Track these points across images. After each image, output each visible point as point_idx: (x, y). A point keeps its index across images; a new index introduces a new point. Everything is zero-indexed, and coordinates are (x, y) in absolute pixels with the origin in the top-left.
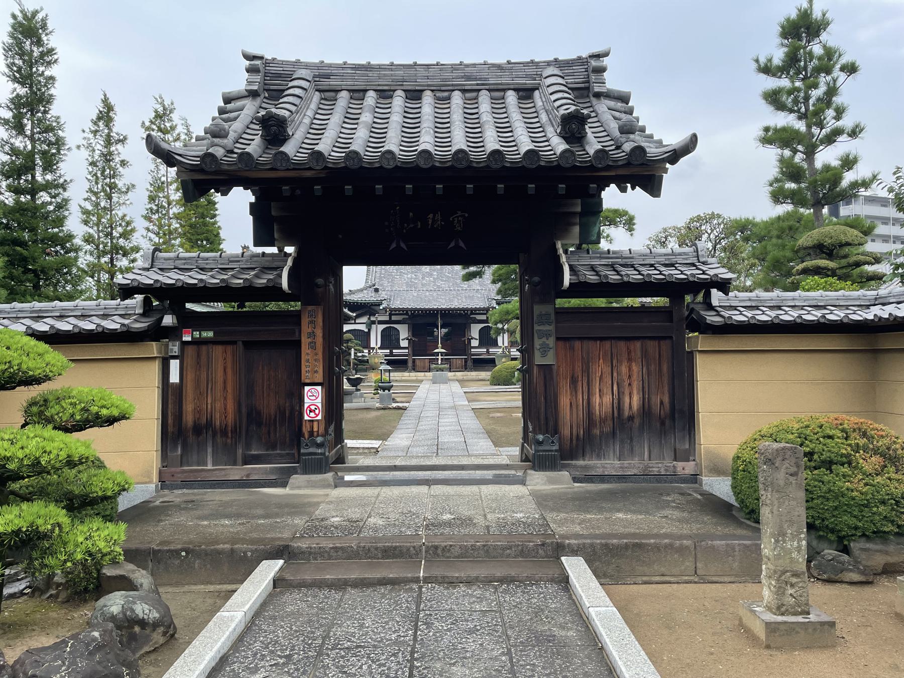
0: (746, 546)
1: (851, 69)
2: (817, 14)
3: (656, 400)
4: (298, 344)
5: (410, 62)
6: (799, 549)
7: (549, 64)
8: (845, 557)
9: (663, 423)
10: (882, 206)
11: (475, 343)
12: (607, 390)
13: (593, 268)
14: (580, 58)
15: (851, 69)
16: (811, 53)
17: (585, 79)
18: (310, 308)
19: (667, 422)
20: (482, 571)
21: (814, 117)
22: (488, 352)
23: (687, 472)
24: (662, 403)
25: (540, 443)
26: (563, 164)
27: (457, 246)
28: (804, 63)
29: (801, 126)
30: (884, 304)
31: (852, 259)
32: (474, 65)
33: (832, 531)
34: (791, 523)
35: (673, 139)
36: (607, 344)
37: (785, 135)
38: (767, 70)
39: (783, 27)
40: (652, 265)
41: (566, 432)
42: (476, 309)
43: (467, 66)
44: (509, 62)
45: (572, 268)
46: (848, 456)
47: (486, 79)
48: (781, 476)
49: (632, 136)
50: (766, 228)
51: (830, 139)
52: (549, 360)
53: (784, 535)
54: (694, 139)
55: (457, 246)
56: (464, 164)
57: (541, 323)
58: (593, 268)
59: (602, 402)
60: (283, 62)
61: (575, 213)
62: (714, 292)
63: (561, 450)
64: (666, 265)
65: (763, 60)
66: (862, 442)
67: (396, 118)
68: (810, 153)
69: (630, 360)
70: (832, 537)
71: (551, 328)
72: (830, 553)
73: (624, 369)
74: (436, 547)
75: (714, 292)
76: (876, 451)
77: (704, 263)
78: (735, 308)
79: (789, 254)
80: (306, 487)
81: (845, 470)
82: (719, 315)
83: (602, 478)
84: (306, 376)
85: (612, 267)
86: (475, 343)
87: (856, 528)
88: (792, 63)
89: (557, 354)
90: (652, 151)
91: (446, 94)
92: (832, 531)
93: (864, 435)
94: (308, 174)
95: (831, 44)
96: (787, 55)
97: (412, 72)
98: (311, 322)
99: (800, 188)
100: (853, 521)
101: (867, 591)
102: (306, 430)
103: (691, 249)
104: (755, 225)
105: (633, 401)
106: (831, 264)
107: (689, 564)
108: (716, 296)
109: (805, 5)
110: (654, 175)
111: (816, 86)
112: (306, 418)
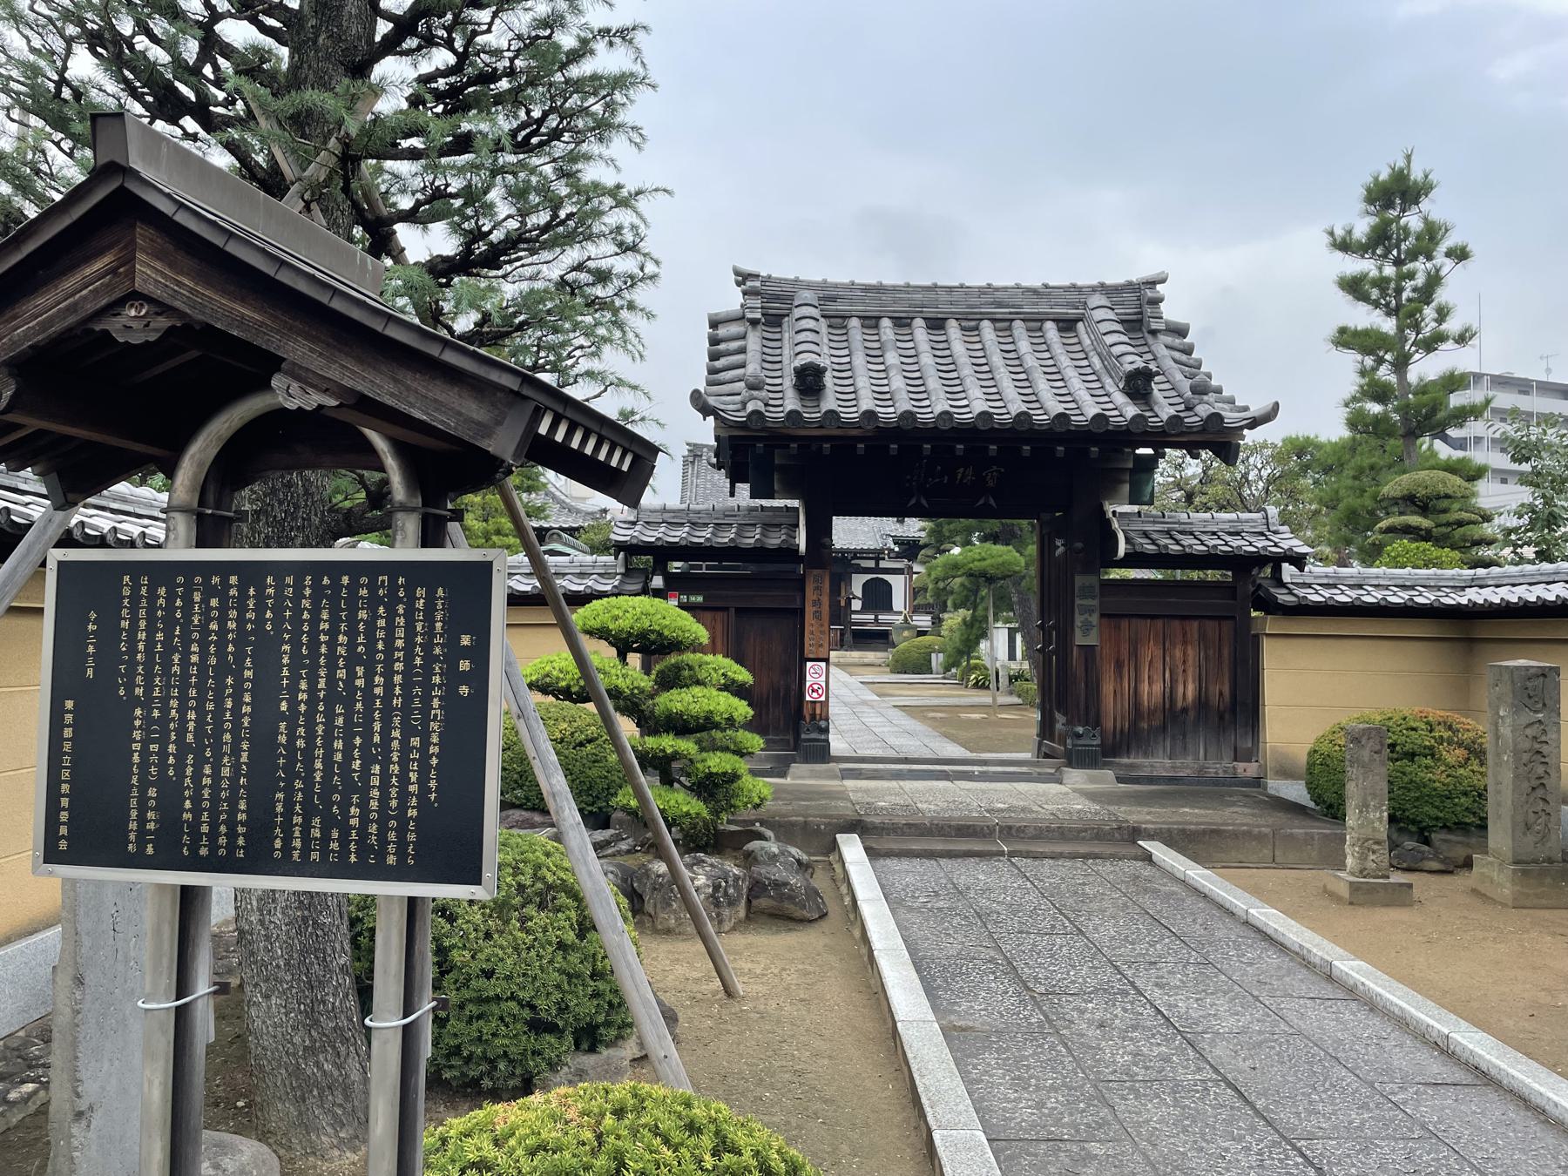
0: (1326, 836)
1: (1459, 254)
2: (1416, 174)
3: (1214, 690)
4: (802, 611)
5: (928, 283)
6: (1380, 819)
7: (1094, 289)
8: (1426, 848)
9: (1221, 718)
10: (1521, 392)
11: (856, 605)
12: (1158, 677)
13: (1146, 534)
14: (1130, 284)
15: (1459, 254)
16: (1406, 229)
17: (1138, 308)
18: (816, 572)
19: (1227, 716)
20: (1066, 848)
21: (1407, 315)
22: (876, 619)
23: (1248, 774)
24: (1221, 694)
25: (1079, 736)
26: (1133, 429)
27: (986, 504)
28: (1396, 236)
29: (1388, 325)
30: (1481, 587)
31: (1454, 516)
32: (1005, 289)
33: (1414, 822)
34: (1374, 795)
35: (1257, 407)
36: (1159, 623)
37: (1369, 342)
38: (1344, 245)
39: (1369, 190)
40: (1214, 533)
41: (1109, 724)
42: (862, 551)
43: (997, 289)
44: (1046, 286)
45: (1128, 540)
46: (1431, 748)
47: (1020, 307)
48: (1366, 754)
49: (1205, 398)
50: (1335, 453)
51: (1430, 345)
52: (1092, 640)
53: (1367, 806)
54: (1276, 407)
55: (986, 504)
56: (1027, 426)
57: (1084, 597)
58: (1146, 534)
59: (1151, 691)
60: (780, 281)
61: (1124, 470)
62: (1285, 566)
63: (1102, 745)
64: (1230, 534)
65: (1339, 232)
66: (1446, 735)
67: (927, 359)
68: (1401, 364)
69: (1185, 643)
70: (1413, 828)
71: (1095, 602)
72: (1410, 844)
73: (1178, 653)
74: (1010, 828)
75: (1285, 566)
76: (1460, 744)
77: (1275, 532)
78: (1310, 586)
79: (1368, 502)
80: (810, 777)
81: (1429, 761)
82: (1291, 593)
83: (1151, 780)
84: (809, 650)
85: (1168, 533)
86: (856, 605)
87: (1437, 819)
88: (1381, 240)
89: (1101, 634)
90: (1230, 417)
91: (973, 324)
92: (1414, 822)
93: (1450, 728)
94: (854, 432)
95: (1435, 216)
96: (1374, 229)
97: (932, 296)
98: (817, 588)
99: (1386, 412)
100: (1434, 812)
101: (1447, 879)
102: (807, 712)
103: (1259, 515)
104: (1319, 446)
105: (1188, 691)
106: (1425, 523)
107: (1267, 852)
108: (1288, 571)
109: (1401, 163)
110: (1229, 443)
111: (1411, 275)
112: (808, 698)
